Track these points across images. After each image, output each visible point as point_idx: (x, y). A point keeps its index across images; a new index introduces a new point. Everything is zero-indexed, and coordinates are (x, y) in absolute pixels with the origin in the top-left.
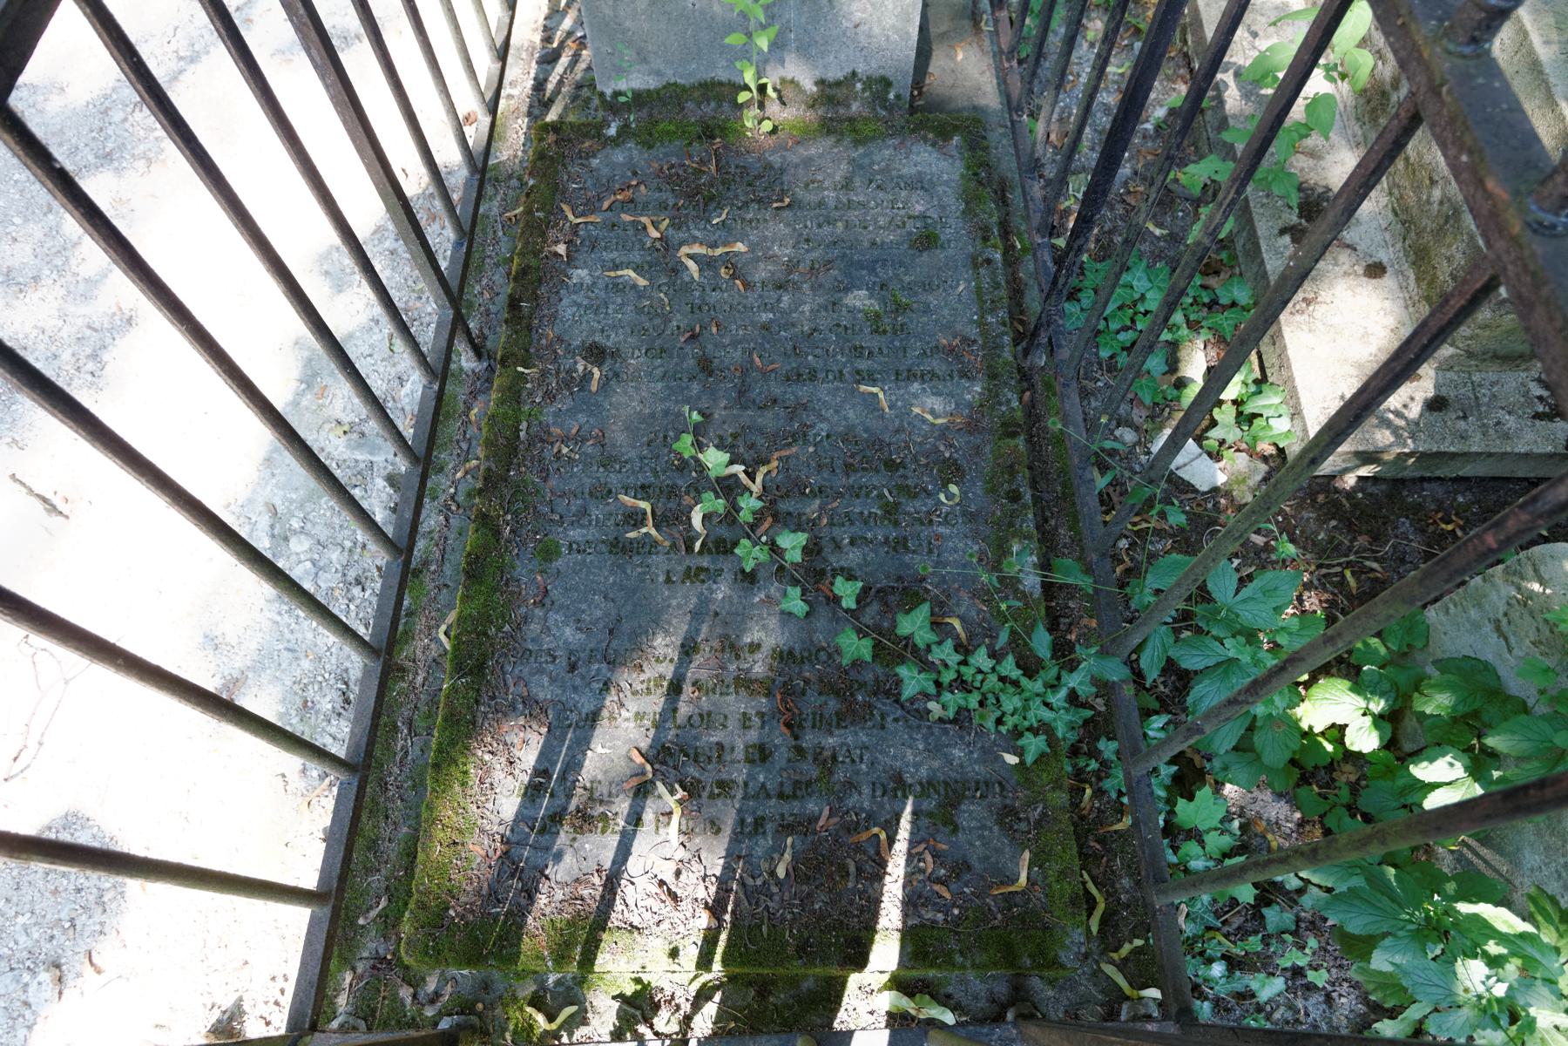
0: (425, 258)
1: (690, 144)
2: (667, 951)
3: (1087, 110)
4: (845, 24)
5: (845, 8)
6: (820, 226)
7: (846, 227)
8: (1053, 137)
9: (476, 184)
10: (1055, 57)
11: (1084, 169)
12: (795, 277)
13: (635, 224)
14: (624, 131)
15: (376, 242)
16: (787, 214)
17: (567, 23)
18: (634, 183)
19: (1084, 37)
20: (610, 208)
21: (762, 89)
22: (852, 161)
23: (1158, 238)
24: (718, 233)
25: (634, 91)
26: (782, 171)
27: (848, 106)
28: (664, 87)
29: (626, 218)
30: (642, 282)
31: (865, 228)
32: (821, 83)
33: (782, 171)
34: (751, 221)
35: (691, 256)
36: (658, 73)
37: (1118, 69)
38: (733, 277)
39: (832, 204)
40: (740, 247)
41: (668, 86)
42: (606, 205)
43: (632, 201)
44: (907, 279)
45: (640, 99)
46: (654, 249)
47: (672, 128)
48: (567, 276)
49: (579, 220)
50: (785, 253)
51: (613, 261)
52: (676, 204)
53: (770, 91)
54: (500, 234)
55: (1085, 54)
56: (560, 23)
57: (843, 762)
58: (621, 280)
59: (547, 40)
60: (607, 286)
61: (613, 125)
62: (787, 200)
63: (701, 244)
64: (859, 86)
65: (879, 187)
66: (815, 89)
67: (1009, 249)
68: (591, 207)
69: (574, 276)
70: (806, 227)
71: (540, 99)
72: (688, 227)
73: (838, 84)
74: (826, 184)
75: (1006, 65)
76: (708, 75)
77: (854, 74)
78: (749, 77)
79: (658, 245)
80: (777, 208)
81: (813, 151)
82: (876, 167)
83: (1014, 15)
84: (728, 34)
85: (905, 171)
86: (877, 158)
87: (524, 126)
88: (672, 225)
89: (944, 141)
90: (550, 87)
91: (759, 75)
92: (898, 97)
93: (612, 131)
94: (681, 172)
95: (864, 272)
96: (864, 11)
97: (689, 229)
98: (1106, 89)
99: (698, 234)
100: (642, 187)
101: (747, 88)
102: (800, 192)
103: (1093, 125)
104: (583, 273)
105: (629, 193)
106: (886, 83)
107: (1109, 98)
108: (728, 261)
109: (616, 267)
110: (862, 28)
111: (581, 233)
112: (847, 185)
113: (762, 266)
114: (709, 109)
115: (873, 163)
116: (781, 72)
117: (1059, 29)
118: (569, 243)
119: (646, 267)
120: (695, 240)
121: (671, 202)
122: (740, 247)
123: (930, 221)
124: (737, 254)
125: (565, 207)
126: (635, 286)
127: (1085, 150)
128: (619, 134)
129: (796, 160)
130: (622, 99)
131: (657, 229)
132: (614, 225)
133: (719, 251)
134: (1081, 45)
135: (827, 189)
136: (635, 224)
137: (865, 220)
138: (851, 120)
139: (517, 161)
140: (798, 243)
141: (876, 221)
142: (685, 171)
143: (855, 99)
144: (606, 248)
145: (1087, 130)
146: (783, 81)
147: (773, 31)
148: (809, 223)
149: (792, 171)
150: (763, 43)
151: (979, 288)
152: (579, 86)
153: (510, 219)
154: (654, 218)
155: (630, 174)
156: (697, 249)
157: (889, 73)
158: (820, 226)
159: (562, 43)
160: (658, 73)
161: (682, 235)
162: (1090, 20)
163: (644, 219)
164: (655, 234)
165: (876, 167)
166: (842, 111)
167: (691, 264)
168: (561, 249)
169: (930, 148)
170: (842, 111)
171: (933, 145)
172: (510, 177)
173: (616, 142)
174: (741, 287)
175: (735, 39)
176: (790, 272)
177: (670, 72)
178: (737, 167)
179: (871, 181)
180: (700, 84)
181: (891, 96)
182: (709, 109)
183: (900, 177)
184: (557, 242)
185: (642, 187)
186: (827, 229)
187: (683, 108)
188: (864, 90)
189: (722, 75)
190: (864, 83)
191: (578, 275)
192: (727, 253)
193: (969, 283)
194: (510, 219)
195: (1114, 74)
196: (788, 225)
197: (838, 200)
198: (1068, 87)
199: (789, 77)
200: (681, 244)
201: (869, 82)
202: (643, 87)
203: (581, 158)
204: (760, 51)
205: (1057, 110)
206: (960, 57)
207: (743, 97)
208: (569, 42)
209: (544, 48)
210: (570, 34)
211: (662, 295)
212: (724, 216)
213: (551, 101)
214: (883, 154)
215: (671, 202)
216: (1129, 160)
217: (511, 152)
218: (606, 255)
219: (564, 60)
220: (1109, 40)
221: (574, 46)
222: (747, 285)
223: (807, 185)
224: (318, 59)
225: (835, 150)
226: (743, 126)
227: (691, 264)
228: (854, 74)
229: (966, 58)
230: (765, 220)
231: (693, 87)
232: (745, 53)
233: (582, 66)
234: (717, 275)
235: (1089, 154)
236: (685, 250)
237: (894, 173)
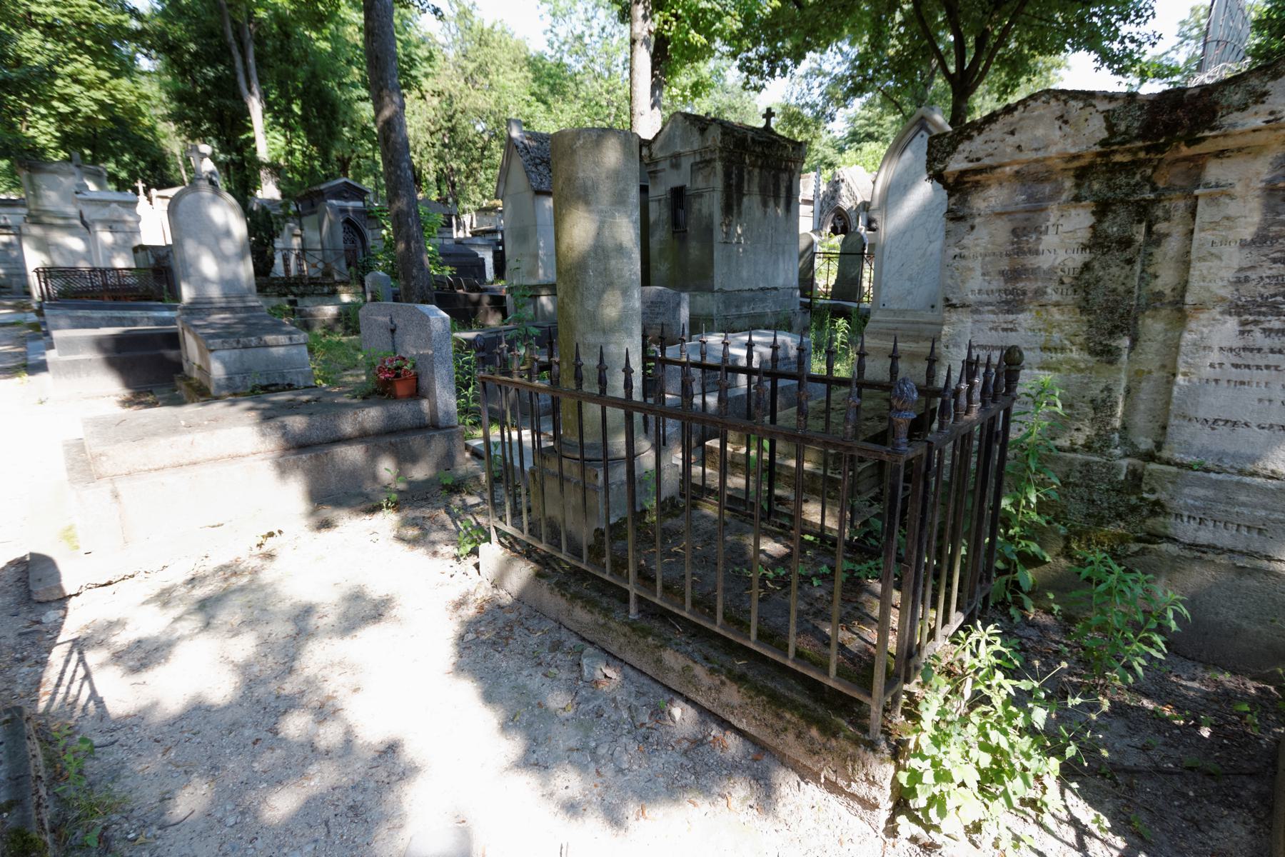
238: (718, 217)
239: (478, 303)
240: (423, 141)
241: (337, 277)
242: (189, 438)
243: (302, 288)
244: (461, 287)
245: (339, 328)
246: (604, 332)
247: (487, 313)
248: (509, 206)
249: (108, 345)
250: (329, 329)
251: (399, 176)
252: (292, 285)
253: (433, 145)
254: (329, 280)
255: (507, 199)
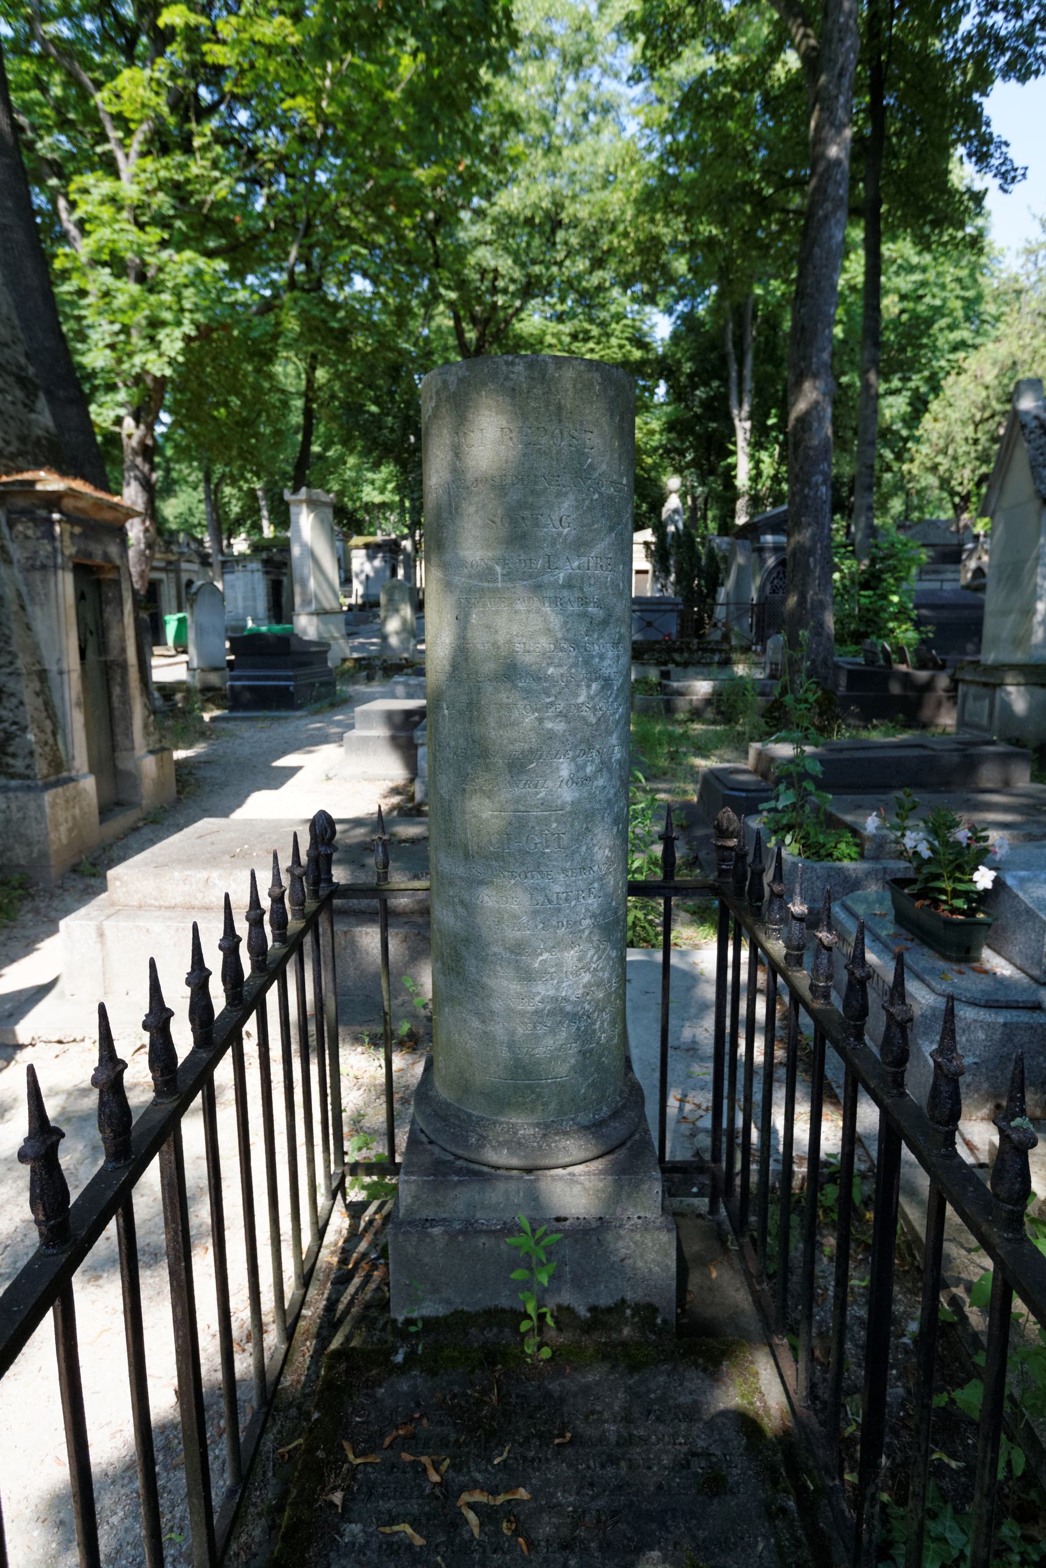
0: (203, 1515)
1: (472, 1371)
2: (1020, 85)
3: (842, 1328)
4: (613, 1258)
5: (612, 1246)
6: (603, 1466)
7: (630, 1467)
8: (817, 1353)
9: (262, 1417)
10: (800, 1271)
11: (856, 1390)
12: (581, 1533)
13: (415, 1464)
14: (410, 1357)
15: (126, 1481)
16: (569, 1451)
17: (363, 1246)
18: (417, 1415)
19: (822, 1252)
20: (390, 1446)
21: (541, 1317)
22: (629, 1389)
23: (956, 1472)
24: (500, 1475)
25: (423, 1318)
26: (562, 1400)
27: (620, 1331)
28: (452, 1314)
29: (407, 1457)
30: (419, 1541)
31: (649, 1468)
32: (593, 1309)
33: (562, 1400)
34: (532, 1461)
35: (471, 1506)
36: (448, 1302)
37: (858, 1282)
38: (516, 1533)
39: (613, 1439)
40: (523, 1494)
41: (455, 1313)
42: (387, 1441)
43: (413, 1436)
44: (701, 1534)
45: (430, 1324)
46: (433, 1496)
47: (456, 1353)
48: (338, 1533)
49: (359, 1461)
50: (567, 1499)
51: (389, 1511)
52: (457, 1441)
53: (549, 1320)
54: (270, 1474)
55: (825, 1266)
56: (356, 1247)
57: (760, 550)
58: (396, 1538)
59: (343, 1261)
60: (380, 1547)
61: (401, 1351)
62: (569, 1435)
63: (482, 1490)
64: (628, 1312)
65: (658, 1418)
66: (588, 1315)
67: (800, 1491)
68: (372, 1445)
69: (347, 1533)
70: (589, 1467)
71: (330, 1322)
72: (469, 1468)
73: (609, 1310)
74: (606, 1415)
75: (758, 1288)
76: (491, 1304)
77: (623, 1301)
78: (531, 1309)
79: (437, 1491)
80: (559, 1445)
81: (590, 1378)
82: (652, 1396)
83: (755, 1234)
84: (513, 1270)
85: (682, 1400)
86: (652, 1385)
87: (311, 1349)
88: (452, 1466)
89: (634, 643)
90: (341, 1307)
91: (539, 1307)
92: (664, 1321)
93: (399, 1358)
94: (463, 1403)
95: (654, 1526)
96: (628, 1248)
97: (469, 1471)
98: (855, 1302)
99: (478, 1476)
100: (425, 1421)
101: (529, 1317)
102: (581, 1426)
103: (853, 1339)
104: (356, 1528)
105: (411, 1428)
106: (652, 1309)
107: (858, 1311)
108: (510, 1510)
109: (393, 1521)
110: (627, 1262)
111: (359, 1476)
112: (627, 1419)
113: (547, 1519)
114: (490, 1334)
115: (649, 1391)
116: (558, 1300)
117: (797, 1247)
118: (348, 1491)
119: (424, 1521)
120: (475, 1485)
121: (453, 1437)
122: (523, 1494)
123: (714, 1460)
124: (520, 1502)
125: (346, 1445)
126: (411, 1546)
127: (853, 1367)
128: (406, 1359)
129: (574, 1389)
130: (413, 1329)
131: (437, 1470)
132: (393, 1466)
133: (501, 1499)
134: (821, 1260)
135: (606, 1421)
136: (415, 1464)
137: (649, 1459)
138: (624, 1344)
139: (299, 1387)
140: (581, 1488)
141: (660, 1461)
142: (467, 1402)
143: (626, 1324)
144: (383, 1495)
145: (848, 1345)
146: (560, 1307)
147: (551, 1268)
148: (591, 1463)
149: (571, 1400)
150: (544, 1279)
151: (778, 1545)
152: (368, 1306)
153: (283, 1456)
154: (434, 1457)
155: (412, 1405)
156: (479, 1497)
157: (655, 1301)
158: (603, 1466)
159: (357, 1264)
160: (448, 1302)
161: (463, 1479)
162: (823, 1236)
163: (425, 1459)
164: (435, 1478)
165: (652, 1396)
166: (614, 1336)
167: (471, 1516)
168: (337, 1498)
169: (701, 1374)
170: (614, 1336)
171: (705, 1370)
172: (290, 1405)
173: (402, 1369)
174: (524, 1548)
175: (518, 1275)
176: (575, 1526)
177: (458, 1300)
178: (518, 1396)
179: (649, 1412)
180: (485, 1312)
181: (659, 1321)
182: (490, 1334)
183: (678, 1406)
184: (334, 1489)
185: (425, 1421)
186: (610, 1470)
187: (467, 1334)
188: (633, 1316)
189: (504, 1302)
190: (633, 1309)
191: (351, 1531)
192: (509, 1501)
193: (768, 1540)
194: (283, 1456)
195: (859, 1287)
196: (570, 1465)
197: (620, 1436)
198: (820, 1300)
199: (566, 1304)
200: (462, 1490)
201: (637, 1308)
202: (433, 1314)
203: (367, 1387)
204: (540, 1284)
205: (815, 1325)
206: (714, 1275)
207: (524, 1326)
208: (363, 1264)
209: (339, 1269)
210: (364, 1255)
211: (439, 1558)
212: (505, 1455)
213: (340, 1322)
214: (658, 1380)
215: (453, 1437)
216: (899, 1378)
217: (295, 1377)
218: (384, 1505)
219: (357, 1281)
220: (842, 1257)
221: (367, 1267)
222: (531, 1544)
223: (587, 1417)
224: (179, 1314)
225: (611, 1377)
226: (523, 1352)
227: (471, 1516)
228: (623, 1301)
229: (719, 1276)
230: (547, 1460)
231: (477, 1314)
232: (526, 1285)
233: (372, 1286)
234: (499, 1531)
235: (856, 1373)
236: (466, 1497)
237: (671, 1402)
238: (369, 539)
239: (929, 686)
240: (959, 437)
241: (734, 642)
242: (203, 875)
243: (686, 655)
244: (903, 661)
245: (709, 714)
246: (467, 856)
247: (939, 704)
248: (1000, 528)
249: (398, 720)
250: (696, 714)
251: (806, 497)
252: (676, 650)
253: (976, 442)
254: (726, 647)
255: (999, 516)
